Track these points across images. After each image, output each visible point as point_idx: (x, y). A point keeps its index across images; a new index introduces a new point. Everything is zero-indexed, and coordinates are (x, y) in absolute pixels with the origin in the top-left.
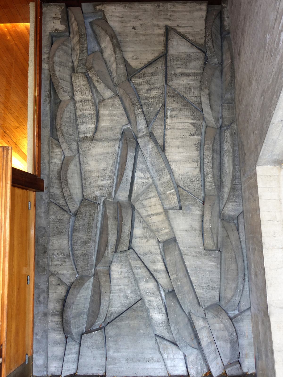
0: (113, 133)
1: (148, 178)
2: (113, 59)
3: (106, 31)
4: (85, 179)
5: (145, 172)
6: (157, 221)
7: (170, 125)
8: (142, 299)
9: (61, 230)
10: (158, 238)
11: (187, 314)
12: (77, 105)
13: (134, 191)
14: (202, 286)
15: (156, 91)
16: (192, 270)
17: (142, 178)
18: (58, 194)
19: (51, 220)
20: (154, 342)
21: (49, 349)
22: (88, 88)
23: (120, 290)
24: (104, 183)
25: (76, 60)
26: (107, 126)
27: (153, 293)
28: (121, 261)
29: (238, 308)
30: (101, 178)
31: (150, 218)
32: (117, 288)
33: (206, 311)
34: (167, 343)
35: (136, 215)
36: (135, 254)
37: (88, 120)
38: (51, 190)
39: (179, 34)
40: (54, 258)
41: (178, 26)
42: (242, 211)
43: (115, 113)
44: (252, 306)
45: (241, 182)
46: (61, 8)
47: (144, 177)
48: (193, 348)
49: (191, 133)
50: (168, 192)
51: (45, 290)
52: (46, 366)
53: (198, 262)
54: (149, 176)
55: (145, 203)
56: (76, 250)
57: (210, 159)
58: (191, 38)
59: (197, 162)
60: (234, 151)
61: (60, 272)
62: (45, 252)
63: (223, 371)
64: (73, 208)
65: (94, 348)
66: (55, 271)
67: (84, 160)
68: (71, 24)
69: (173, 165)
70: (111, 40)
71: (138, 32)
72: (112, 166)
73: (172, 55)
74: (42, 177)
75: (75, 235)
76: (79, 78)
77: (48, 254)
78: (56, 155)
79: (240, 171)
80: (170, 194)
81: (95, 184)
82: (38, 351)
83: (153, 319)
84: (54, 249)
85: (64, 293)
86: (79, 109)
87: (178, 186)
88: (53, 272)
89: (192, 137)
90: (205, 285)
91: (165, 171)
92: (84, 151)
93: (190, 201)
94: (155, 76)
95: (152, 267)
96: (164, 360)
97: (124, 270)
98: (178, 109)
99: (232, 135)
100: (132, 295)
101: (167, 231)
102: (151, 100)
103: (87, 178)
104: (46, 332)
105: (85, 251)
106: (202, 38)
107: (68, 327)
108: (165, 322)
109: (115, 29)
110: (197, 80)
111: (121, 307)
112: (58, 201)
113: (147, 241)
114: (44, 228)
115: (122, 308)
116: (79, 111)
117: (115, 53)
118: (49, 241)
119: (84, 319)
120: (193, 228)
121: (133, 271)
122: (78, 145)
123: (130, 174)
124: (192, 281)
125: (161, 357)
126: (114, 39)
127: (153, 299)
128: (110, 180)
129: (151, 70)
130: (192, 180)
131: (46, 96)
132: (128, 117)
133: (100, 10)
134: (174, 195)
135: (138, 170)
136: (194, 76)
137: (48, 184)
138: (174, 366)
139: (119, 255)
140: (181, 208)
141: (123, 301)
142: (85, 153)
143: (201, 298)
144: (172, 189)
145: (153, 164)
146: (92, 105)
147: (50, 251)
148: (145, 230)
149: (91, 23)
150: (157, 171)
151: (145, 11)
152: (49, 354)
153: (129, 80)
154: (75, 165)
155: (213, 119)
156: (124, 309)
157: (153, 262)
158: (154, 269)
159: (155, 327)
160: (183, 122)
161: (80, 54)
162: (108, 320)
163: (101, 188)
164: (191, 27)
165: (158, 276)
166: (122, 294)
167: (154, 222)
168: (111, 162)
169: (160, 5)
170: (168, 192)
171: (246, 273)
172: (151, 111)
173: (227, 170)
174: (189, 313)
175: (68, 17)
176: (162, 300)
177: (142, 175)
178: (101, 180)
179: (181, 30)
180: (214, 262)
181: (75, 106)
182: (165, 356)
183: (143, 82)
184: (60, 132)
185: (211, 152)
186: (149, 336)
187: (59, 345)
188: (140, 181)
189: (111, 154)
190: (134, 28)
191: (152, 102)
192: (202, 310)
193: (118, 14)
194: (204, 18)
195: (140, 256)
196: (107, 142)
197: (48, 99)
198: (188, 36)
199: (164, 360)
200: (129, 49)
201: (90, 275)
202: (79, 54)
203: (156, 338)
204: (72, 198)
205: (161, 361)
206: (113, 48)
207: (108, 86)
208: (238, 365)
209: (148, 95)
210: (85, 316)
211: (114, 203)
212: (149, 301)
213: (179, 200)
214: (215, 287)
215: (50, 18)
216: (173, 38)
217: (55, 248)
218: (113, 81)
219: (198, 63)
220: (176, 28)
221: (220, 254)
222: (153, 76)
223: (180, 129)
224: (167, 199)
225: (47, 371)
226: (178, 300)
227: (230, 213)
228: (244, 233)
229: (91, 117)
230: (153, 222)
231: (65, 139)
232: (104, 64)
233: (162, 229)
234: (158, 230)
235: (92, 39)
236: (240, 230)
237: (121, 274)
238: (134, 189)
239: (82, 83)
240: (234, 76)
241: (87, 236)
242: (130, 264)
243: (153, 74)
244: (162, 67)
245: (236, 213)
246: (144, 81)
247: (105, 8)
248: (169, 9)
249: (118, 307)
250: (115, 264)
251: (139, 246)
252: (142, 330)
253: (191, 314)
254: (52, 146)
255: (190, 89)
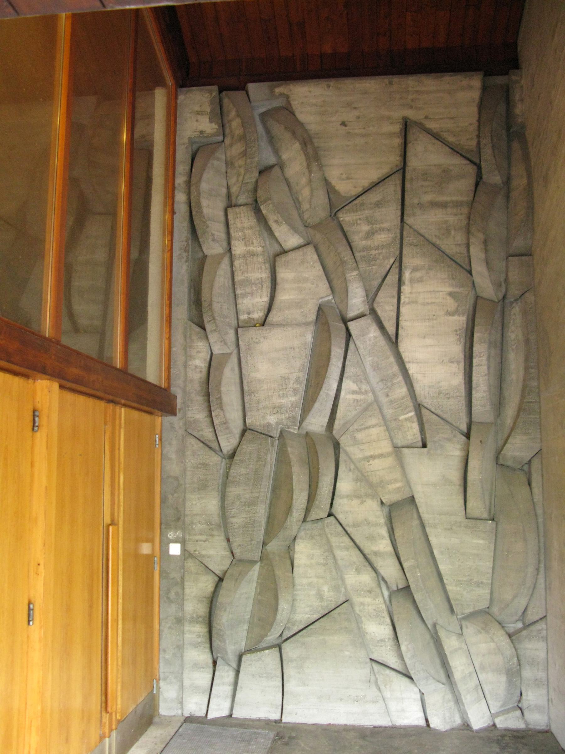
0: (302, 312)
1: (366, 392)
2: (304, 180)
3: (294, 133)
4: (250, 394)
5: (361, 382)
6: (380, 468)
7: (409, 295)
8: (348, 600)
9: (206, 483)
10: (382, 498)
11: (429, 626)
12: (237, 263)
13: (339, 415)
14: (459, 581)
15: (383, 236)
16: (442, 553)
17: (354, 392)
18: (201, 420)
19: (188, 465)
20: (368, 670)
21: (185, 675)
22: (257, 233)
23: (310, 585)
24: (283, 401)
25: (235, 184)
26: (292, 299)
27: (370, 592)
28: (312, 537)
29: (521, 618)
30: (279, 392)
31: (369, 463)
32: (305, 581)
33: (464, 623)
34: (391, 674)
35: (342, 457)
36: (338, 525)
37: (255, 289)
38: (189, 414)
39: (429, 132)
40: (193, 529)
41: (426, 117)
42: (539, 449)
43: (307, 276)
44: (548, 615)
45: (540, 399)
46: (211, 94)
47: (358, 390)
48: (438, 681)
49: (449, 310)
50: (402, 417)
51: (179, 580)
52: (181, 700)
53: (453, 539)
54: (368, 388)
55: (360, 436)
56: (231, 517)
57: (484, 358)
58: (451, 139)
59: (458, 362)
60: (527, 341)
61: (203, 553)
62: (178, 519)
63: (489, 722)
64: (227, 445)
65: (262, 677)
66: (195, 551)
67: (248, 362)
68: (228, 122)
69: (412, 369)
70: (302, 148)
71: (351, 131)
72: (300, 371)
73: (415, 170)
74: (173, 390)
75: (231, 492)
76: (242, 215)
77: (184, 522)
78: (198, 352)
79: (538, 379)
80: (406, 419)
81: (267, 403)
82: (168, 677)
83: (367, 633)
84: (195, 515)
85: (210, 588)
86: (240, 270)
87: (418, 407)
88: (192, 552)
89: (451, 318)
90: (465, 579)
91: (398, 381)
92: (248, 345)
93: (442, 433)
94: (381, 207)
95: (368, 548)
96: (384, 699)
97: (317, 552)
98: (424, 267)
99: (524, 313)
100: (332, 593)
101: (399, 485)
102: (373, 252)
103: (253, 393)
104: (180, 648)
105: (248, 519)
106: (472, 139)
107: (220, 641)
108: (389, 639)
109: (308, 127)
110: (461, 214)
111: (312, 613)
112: (201, 433)
113: (362, 503)
114: (176, 478)
115: (313, 615)
116: (240, 274)
117: (310, 172)
118: (184, 499)
119: (242, 632)
120: (447, 481)
121: (333, 554)
122: (237, 334)
123: (335, 386)
124: (442, 572)
125: (380, 695)
126: (309, 146)
127: (368, 600)
128: (295, 395)
129: (374, 197)
130: (448, 396)
131: (181, 249)
132: (330, 282)
133: (281, 95)
134: (413, 422)
135: (347, 378)
136: (457, 206)
137: (184, 403)
138: (403, 710)
139: (308, 525)
140: (424, 446)
141: (314, 604)
142: (250, 349)
143: (457, 600)
144: (411, 411)
145: (376, 368)
146: (264, 263)
147: (186, 518)
148: (358, 484)
149: (263, 116)
150: (382, 380)
151: (366, 93)
152: (186, 683)
153: (333, 214)
154: (232, 370)
155: (490, 285)
156: (316, 616)
157: (371, 538)
158: (372, 551)
159: (371, 647)
160: (433, 291)
161: (244, 175)
162: (287, 634)
163: (279, 410)
164: (452, 118)
165: (379, 563)
166: (313, 592)
167: (376, 469)
168: (298, 363)
169: (393, 82)
170: (402, 417)
171: (542, 558)
172: (374, 271)
173: (514, 377)
174: (435, 625)
175: (221, 107)
176: (385, 602)
177: (354, 387)
178: (279, 396)
179: (432, 125)
180: (483, 539)
181: (232, 266)
182: (387, 694)
183: (360, 219)
184: (210, 314)
185: (486, 346)
186: (359, 660)
187: (202, 669)
188: (351, 397)
189: (297, 350)
190: (344, 124)
191: (375, 254)
192: (456, 621)
193: (314, 101)
194: (477, 102)
195: (347, 528)
196: (290, 329)
197: (185, 254)
198: (445, 135)
199: (384, 699)
200: (336, 161)
201: (256, 559)
202: (243, 174)
203: (372, 665)
204: (228, 428)
205: (380, 701)
206: (306, 161)
207: (295, 230)
208: (518, 713)
209: (369, 243)
210: (246, 627)
211: (299, 435)
212: (362, 604)
213: (422, 430)
214: (482, 583)
215: (191, 113)
216: (416, 140)
217: (195, 512)
218: (302, 219)
219: (467, 184)
220: (423, 122)
221: (494, 526)
222: (379, 208)
223: (428, 304)
224: (400, 429)
225: (182, 708)
226: (414, 601)
227: (517, 454)
228: (541, 489)
229: (261, 283)
230: (373, 470)
231: (217, 326)
232: (286, 188)
233: (390, 482)
234: (382, 483)
235: (264, 144)
236: (534, 484)
237: (312, 559)
238: (338, 411)
239: (246, 225)
240: (533, 208)
241: (252, 493)
242: (328, 542)
243: (378, 204)
244: (395, 191)
245: (526, 455)
246: (361, 217)
247: (291, 90)
248: (410, 89)
249: (306, 614)
250: (301, 541)
251: (347, 512)
252: (348, 651)
253: (438, 627)
254: (190, 337)
255: (448, 231)
